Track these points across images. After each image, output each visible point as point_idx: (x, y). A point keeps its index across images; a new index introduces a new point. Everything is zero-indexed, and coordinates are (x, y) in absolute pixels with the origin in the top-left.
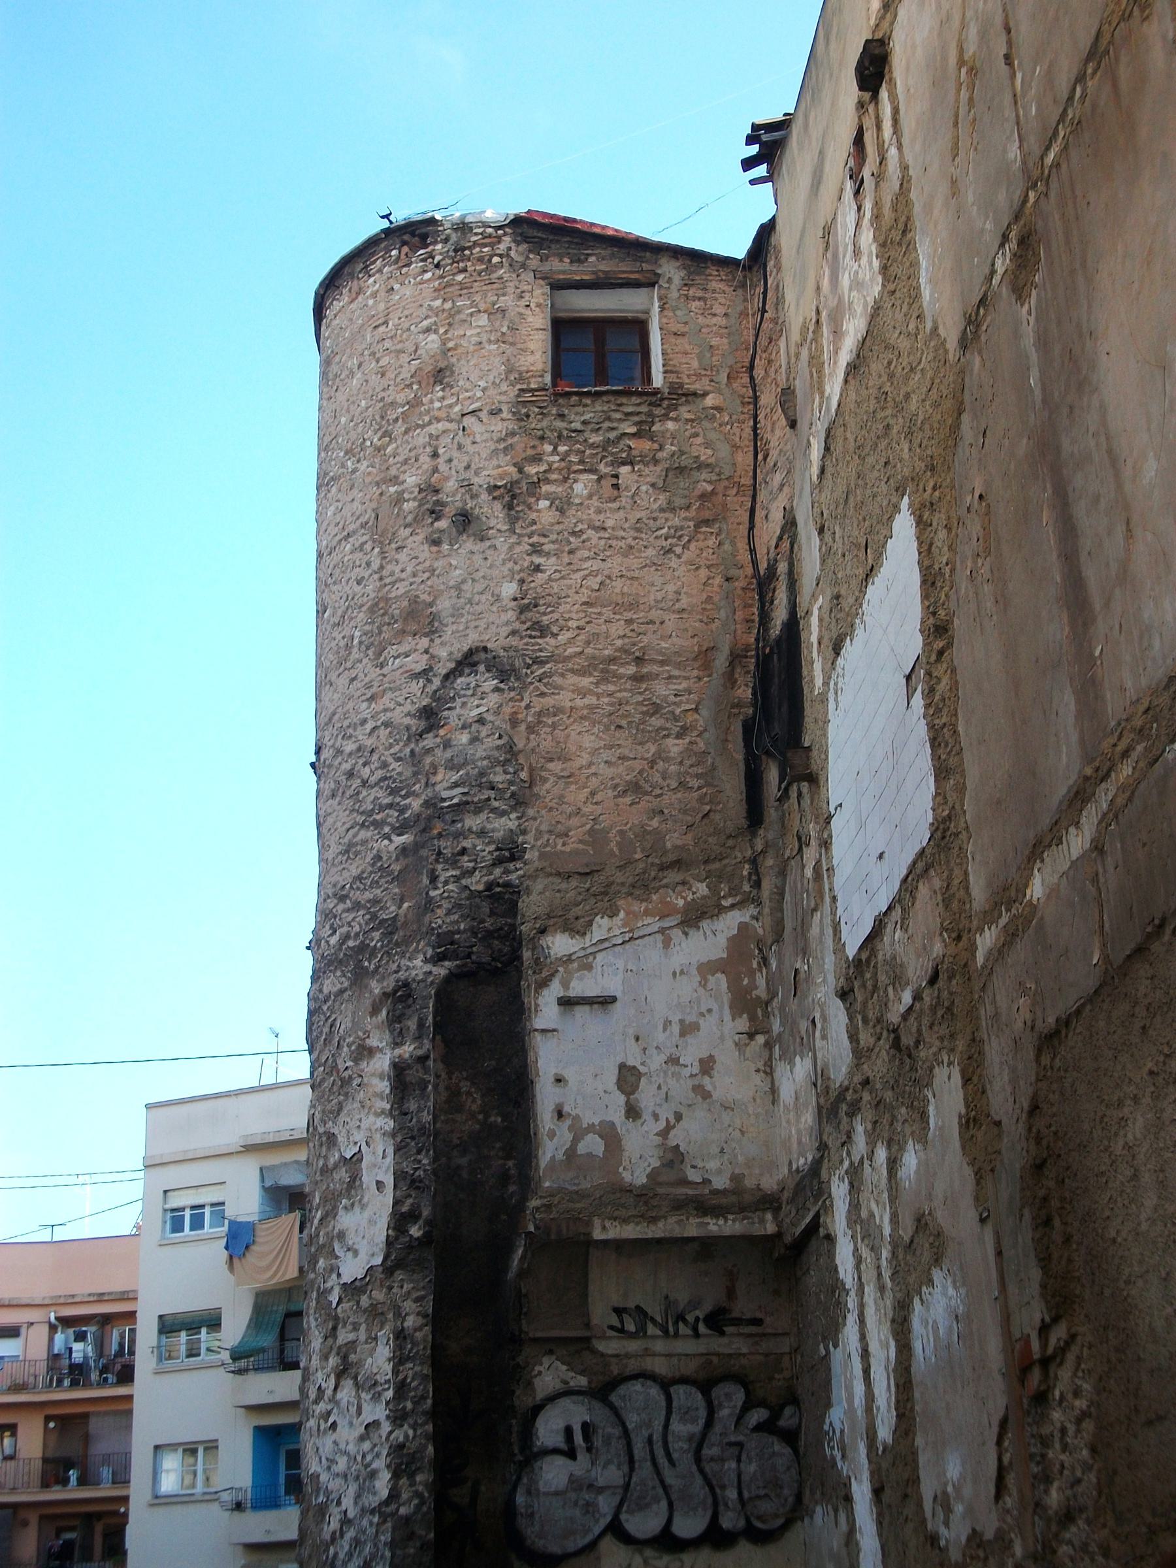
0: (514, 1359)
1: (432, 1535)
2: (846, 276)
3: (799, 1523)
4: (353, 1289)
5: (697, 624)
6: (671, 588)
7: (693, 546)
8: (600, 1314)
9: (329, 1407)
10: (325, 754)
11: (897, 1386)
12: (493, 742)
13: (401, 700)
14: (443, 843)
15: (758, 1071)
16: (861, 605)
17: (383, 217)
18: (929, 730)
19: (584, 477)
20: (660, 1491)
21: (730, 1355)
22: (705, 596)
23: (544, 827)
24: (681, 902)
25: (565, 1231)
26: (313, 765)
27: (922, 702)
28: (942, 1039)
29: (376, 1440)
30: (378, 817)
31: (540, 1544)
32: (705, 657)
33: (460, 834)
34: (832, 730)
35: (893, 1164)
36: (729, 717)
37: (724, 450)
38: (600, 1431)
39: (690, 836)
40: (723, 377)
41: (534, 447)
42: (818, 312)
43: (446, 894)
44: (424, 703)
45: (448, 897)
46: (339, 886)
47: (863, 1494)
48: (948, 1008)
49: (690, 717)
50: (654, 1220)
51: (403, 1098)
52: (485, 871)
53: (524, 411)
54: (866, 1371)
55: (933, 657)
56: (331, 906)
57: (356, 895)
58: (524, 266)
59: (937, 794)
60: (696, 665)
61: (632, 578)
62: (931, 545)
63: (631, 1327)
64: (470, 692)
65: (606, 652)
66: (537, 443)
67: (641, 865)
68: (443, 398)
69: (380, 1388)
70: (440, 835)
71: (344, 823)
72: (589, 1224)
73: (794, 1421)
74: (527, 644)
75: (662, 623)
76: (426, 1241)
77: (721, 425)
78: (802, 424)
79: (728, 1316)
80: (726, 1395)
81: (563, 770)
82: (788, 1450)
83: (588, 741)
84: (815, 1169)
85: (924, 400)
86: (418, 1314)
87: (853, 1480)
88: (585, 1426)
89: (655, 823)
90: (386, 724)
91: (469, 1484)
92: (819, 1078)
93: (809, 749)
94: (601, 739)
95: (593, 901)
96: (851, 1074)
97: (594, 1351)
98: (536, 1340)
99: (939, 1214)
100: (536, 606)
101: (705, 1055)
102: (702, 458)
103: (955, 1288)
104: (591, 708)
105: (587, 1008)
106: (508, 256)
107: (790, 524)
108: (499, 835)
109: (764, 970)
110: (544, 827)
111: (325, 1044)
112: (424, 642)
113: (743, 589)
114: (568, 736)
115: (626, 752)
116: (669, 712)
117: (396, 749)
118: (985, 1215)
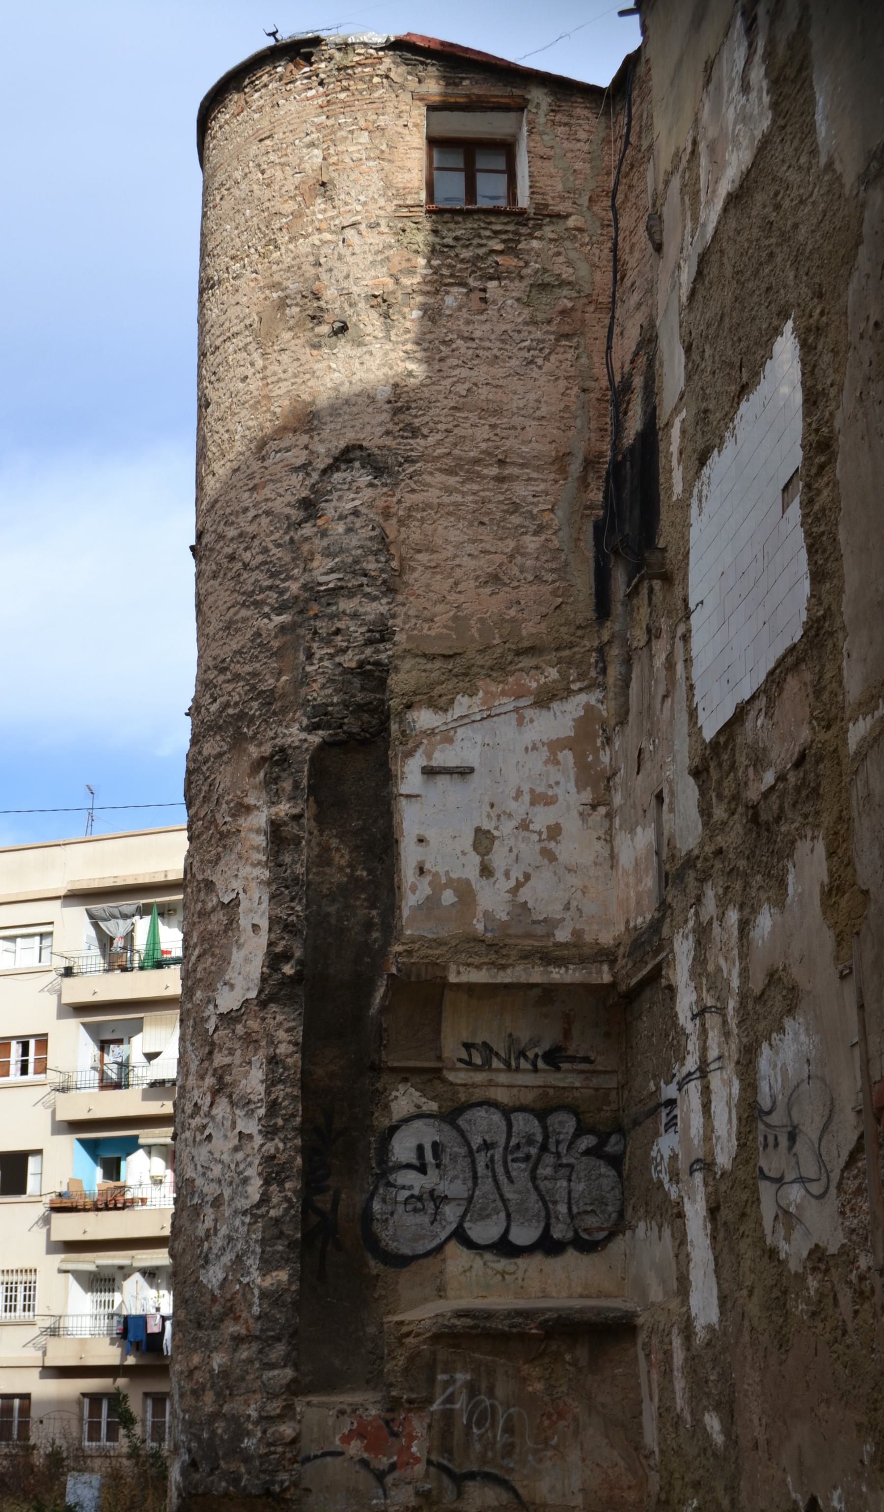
0: (373, 1085)
1: (299, 1235)
2: (732, 109)
3: (621, 1236)
4: (229, 1019)
5: (555, 431)
6: (532, 396)
7: (553, 358)
8: (451, 1049)
9: (205, 1121)
10: (207, 539)
11: (740, 1119)
12: (366, 533)
13: (281, 491)
14: (318, 624)
15: (599, 838)
16: (732, 420)
17: (269, 35)
18: (806, 537)
19: (455, 290)
20: (500, 1204)
21: (564, 1088)
22: (562, 406)
23: (412, 612)
24: (534, 685)
25: (423, 974)
26: (192, 548)
27: (800, 512)
28: (806, 816)
29: (249, 1151)
30: (258, 598)
31: (393, 1245)
32: (561, 462)
33: (335, 616)
34: (694, 534)
35: (744, 925)
36: (582, 518)
37: (584, 270)
38: (448, 1150)
39: (543, 625)
40: (584, 201)
41: (409, 260)
42: (695, 143)
43: (321, 670)
44: (303, 495)
45: (323, 673)
46: (219, 659)
47: (696, 1212)
48: (813, 788)
49: (547, 516)
50: (503, 967)
51: (278, 852)
52: (357, 651)
53: (400, 225)
54: (706, 1107)
55: (814, 471)
56: (211, 677)
57: (236, 668)
58: (402, 87)
59: (813, 596)
60: (554, 468)
61: (497, 386)
62: (815, 366)
63: (478, 1060)
64: (346, 487)
65: (472, 454)
66: (411, 256)
67: (499, 651)
68: (325, 211)
69: (252, 1106)
70: (316, 616)
71: (225, 602)
72: (445, 968)
73: (619, 1148)
74: (399, 444)
75: (523, 429)
76: (297, 979)
77: (582, 246)
78: (671, 249)
79: (564, 1054)
80: (560, 1122)
81: (430, 561)
82: (612, 1173)
83: (454, 536)
84: (655, 926)
85: (813, 231)
86: (290, 1042)
87: (686, 1200)
88: (435, 1145)
89: (512, 612)
90: (268, 513)
91: (331, 1192)
92: (663, 848)
93: (664, 550)
94: (465, 533)
95: (455, 680)
96: (702, 845)
97: (444, 1081)
98: (393, 1070)
99: (794, 970)
100: (408, 408)
101: (552, 822)
102: (564, 276)
103: (808, 1035)
104: (457, 505)
105: (448, 777)
106: (387, 77)
107: (649, 340)
108: (371, 617)
109: (607, 749)
110: (412, 612)
111: (204, 802)
112: (304, 439)
113: (598, 399)
114: (435, 530)
115: (488, 547)
116: (528, 511)
117: (276, 536)
118: (845, 972)
